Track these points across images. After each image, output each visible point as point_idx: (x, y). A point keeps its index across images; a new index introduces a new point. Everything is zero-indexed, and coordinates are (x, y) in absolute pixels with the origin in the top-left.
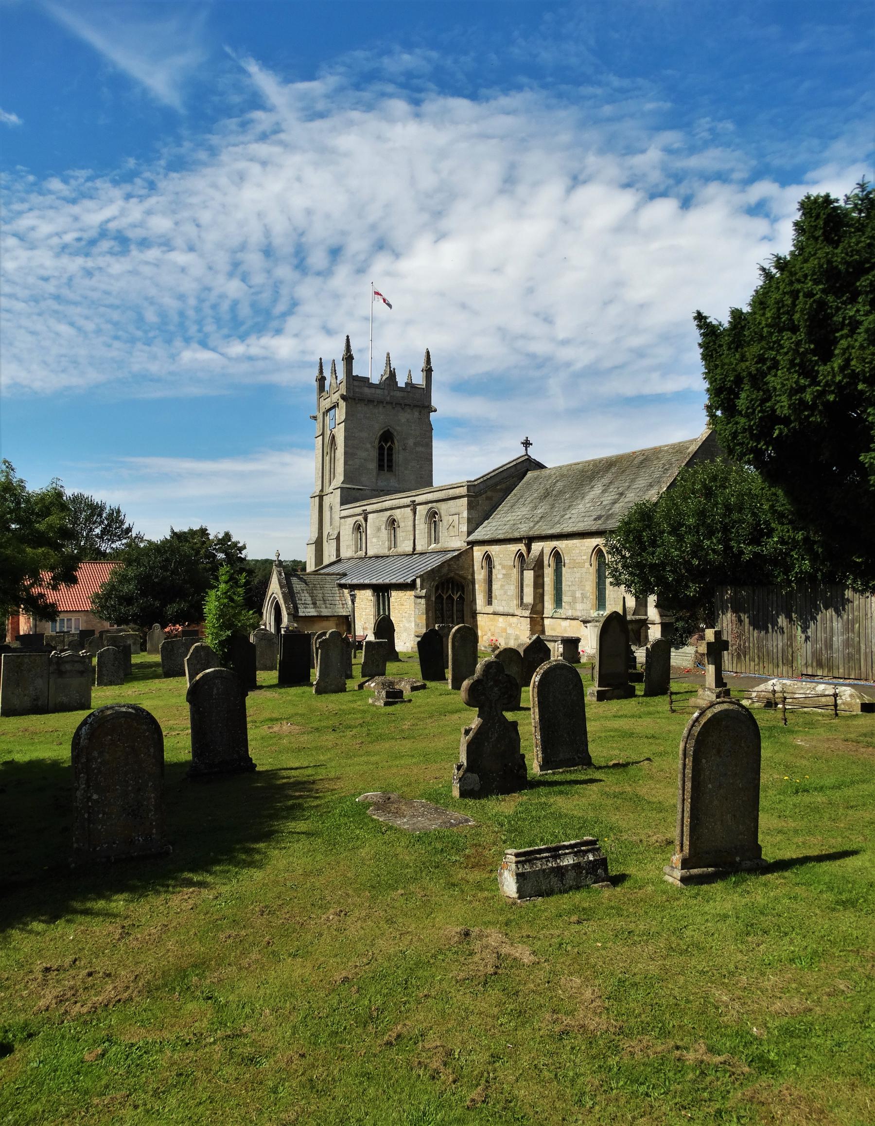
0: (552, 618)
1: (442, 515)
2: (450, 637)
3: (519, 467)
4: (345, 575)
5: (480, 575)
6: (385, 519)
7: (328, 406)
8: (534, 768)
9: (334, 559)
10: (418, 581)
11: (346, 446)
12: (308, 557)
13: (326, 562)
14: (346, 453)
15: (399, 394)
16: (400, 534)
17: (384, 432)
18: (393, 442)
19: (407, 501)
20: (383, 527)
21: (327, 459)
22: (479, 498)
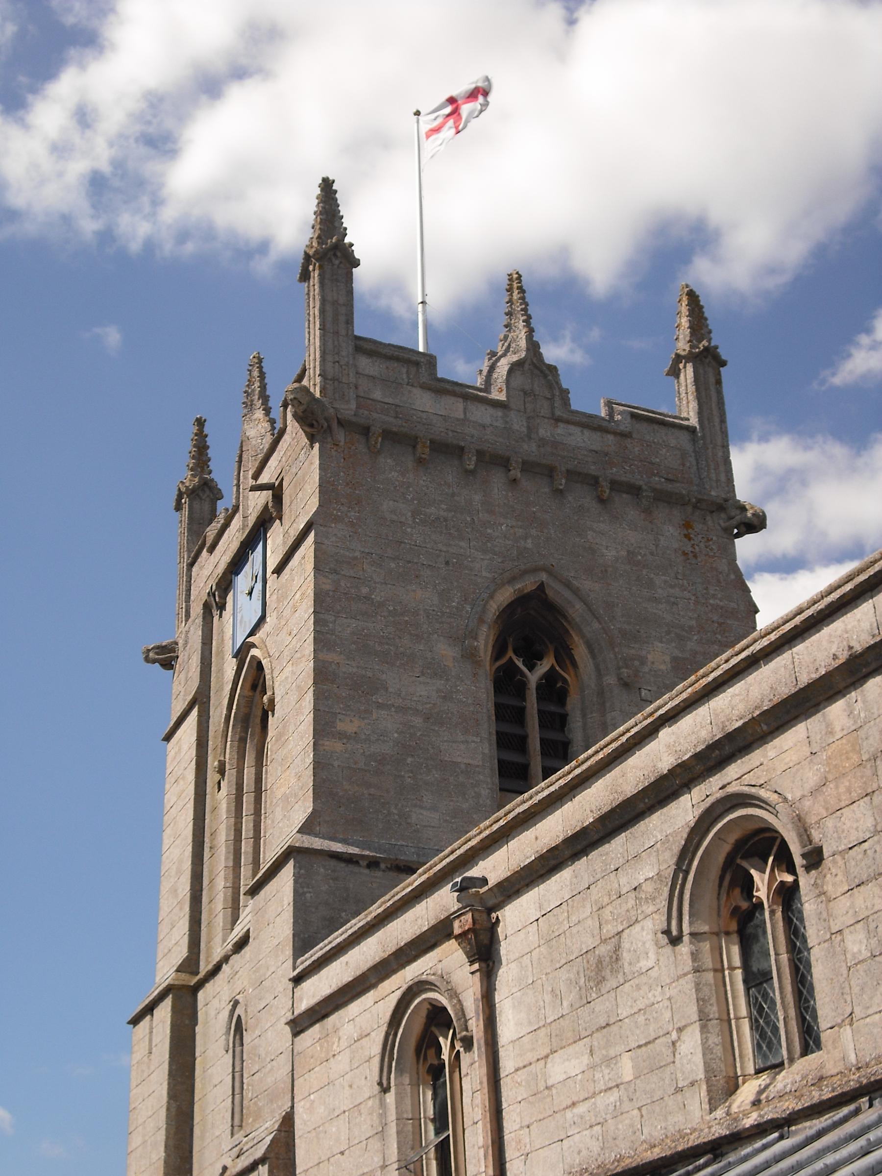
17: (521, 601)
18: (565, 655)
20: (643, 937)
21: (220, 800)
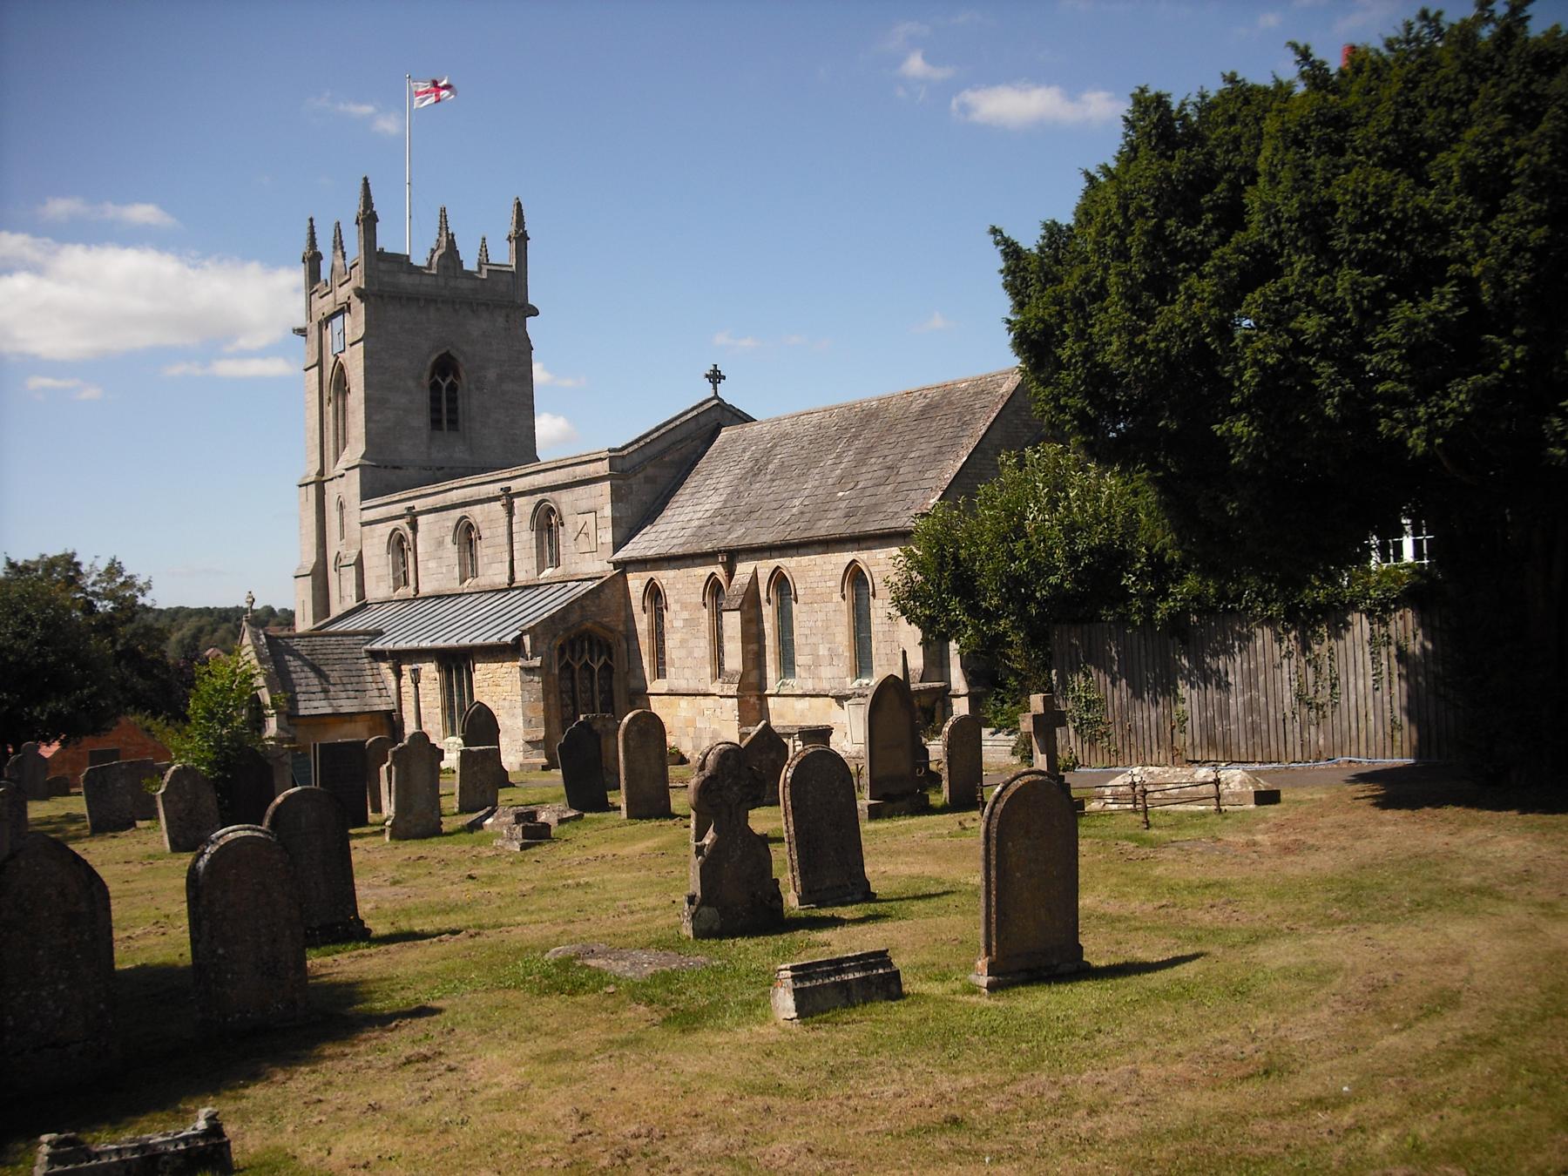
0: (778, 695)
1: (564, 514)
2: (621, 732)
3: (702, 420)
4: (379, 633)
5: (643, 623)
6: (452, 524)
7: (328, 310)
8: (791, 901)
9: (352, 603)
10: (527, 639)
11: (368, 385)
12: (295, 598)
13: (336, 610)
14: (367, 399)
15: (466, 284)
16: (483, 551)
17: (441, 357)
18: (457, 375)
19: (494, 489)
20: (449, 539)
21: (329, 410)
22: (632, 481)
